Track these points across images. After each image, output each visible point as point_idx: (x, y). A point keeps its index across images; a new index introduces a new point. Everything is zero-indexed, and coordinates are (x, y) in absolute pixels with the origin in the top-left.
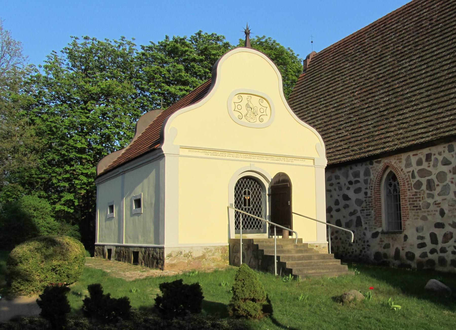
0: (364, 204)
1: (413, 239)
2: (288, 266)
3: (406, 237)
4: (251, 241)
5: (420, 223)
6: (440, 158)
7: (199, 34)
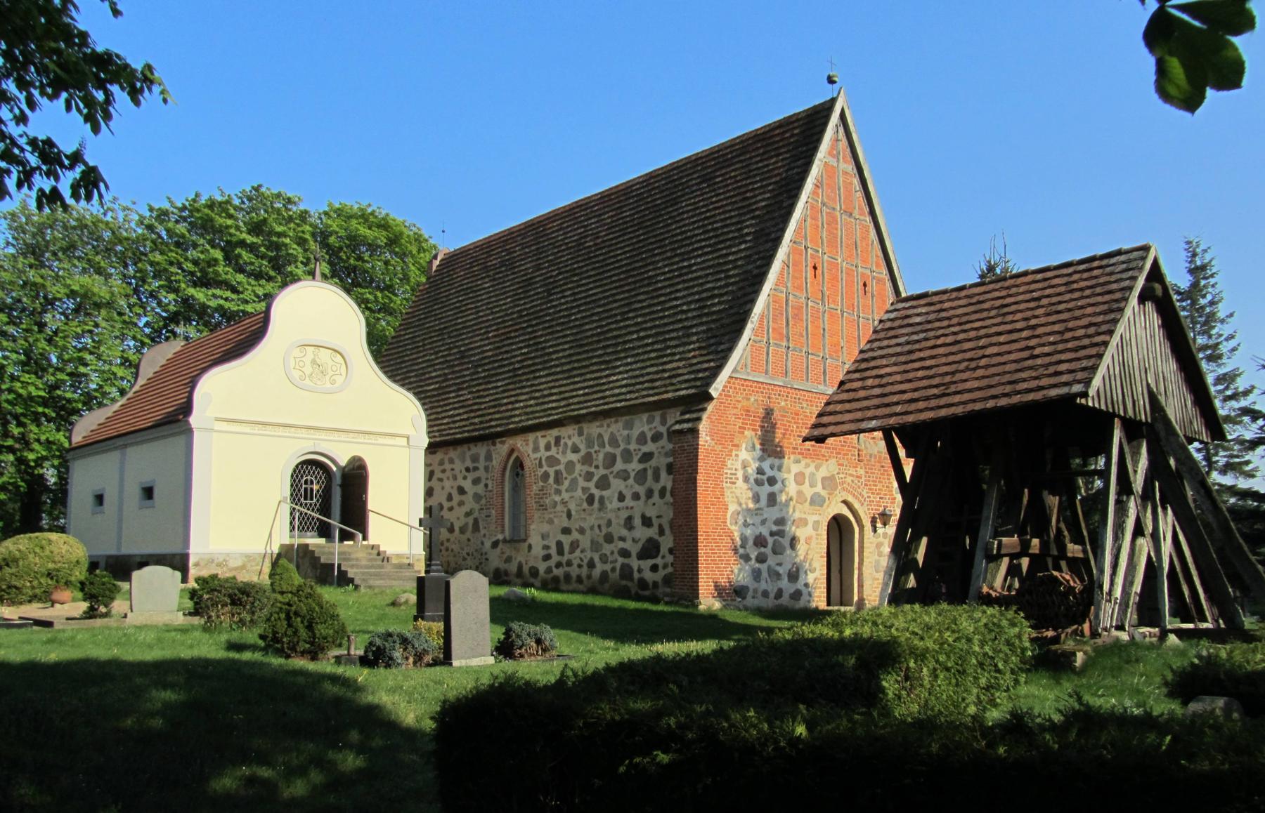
0: (483, 501)
1: (538, 551)
2: (350, 575)
3: (530, 547)
4: (307, 545)
5: (545, 528)
6: (570, 443)
7: (257, 189)
